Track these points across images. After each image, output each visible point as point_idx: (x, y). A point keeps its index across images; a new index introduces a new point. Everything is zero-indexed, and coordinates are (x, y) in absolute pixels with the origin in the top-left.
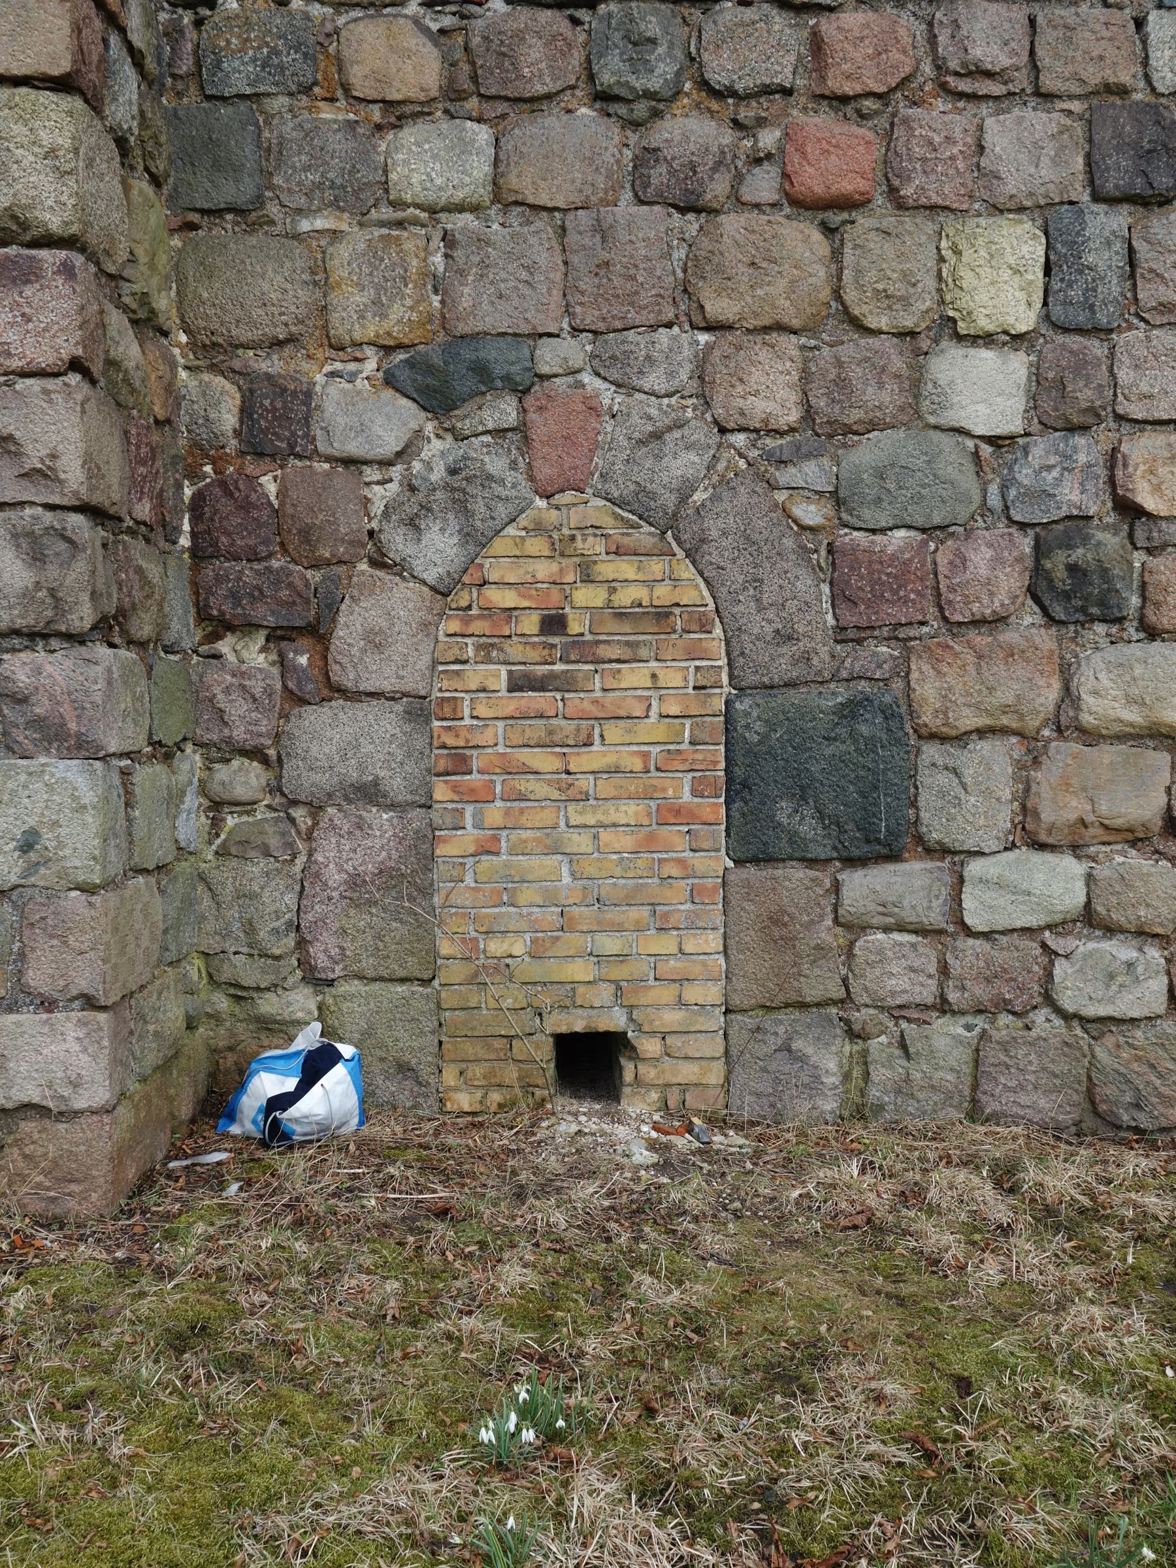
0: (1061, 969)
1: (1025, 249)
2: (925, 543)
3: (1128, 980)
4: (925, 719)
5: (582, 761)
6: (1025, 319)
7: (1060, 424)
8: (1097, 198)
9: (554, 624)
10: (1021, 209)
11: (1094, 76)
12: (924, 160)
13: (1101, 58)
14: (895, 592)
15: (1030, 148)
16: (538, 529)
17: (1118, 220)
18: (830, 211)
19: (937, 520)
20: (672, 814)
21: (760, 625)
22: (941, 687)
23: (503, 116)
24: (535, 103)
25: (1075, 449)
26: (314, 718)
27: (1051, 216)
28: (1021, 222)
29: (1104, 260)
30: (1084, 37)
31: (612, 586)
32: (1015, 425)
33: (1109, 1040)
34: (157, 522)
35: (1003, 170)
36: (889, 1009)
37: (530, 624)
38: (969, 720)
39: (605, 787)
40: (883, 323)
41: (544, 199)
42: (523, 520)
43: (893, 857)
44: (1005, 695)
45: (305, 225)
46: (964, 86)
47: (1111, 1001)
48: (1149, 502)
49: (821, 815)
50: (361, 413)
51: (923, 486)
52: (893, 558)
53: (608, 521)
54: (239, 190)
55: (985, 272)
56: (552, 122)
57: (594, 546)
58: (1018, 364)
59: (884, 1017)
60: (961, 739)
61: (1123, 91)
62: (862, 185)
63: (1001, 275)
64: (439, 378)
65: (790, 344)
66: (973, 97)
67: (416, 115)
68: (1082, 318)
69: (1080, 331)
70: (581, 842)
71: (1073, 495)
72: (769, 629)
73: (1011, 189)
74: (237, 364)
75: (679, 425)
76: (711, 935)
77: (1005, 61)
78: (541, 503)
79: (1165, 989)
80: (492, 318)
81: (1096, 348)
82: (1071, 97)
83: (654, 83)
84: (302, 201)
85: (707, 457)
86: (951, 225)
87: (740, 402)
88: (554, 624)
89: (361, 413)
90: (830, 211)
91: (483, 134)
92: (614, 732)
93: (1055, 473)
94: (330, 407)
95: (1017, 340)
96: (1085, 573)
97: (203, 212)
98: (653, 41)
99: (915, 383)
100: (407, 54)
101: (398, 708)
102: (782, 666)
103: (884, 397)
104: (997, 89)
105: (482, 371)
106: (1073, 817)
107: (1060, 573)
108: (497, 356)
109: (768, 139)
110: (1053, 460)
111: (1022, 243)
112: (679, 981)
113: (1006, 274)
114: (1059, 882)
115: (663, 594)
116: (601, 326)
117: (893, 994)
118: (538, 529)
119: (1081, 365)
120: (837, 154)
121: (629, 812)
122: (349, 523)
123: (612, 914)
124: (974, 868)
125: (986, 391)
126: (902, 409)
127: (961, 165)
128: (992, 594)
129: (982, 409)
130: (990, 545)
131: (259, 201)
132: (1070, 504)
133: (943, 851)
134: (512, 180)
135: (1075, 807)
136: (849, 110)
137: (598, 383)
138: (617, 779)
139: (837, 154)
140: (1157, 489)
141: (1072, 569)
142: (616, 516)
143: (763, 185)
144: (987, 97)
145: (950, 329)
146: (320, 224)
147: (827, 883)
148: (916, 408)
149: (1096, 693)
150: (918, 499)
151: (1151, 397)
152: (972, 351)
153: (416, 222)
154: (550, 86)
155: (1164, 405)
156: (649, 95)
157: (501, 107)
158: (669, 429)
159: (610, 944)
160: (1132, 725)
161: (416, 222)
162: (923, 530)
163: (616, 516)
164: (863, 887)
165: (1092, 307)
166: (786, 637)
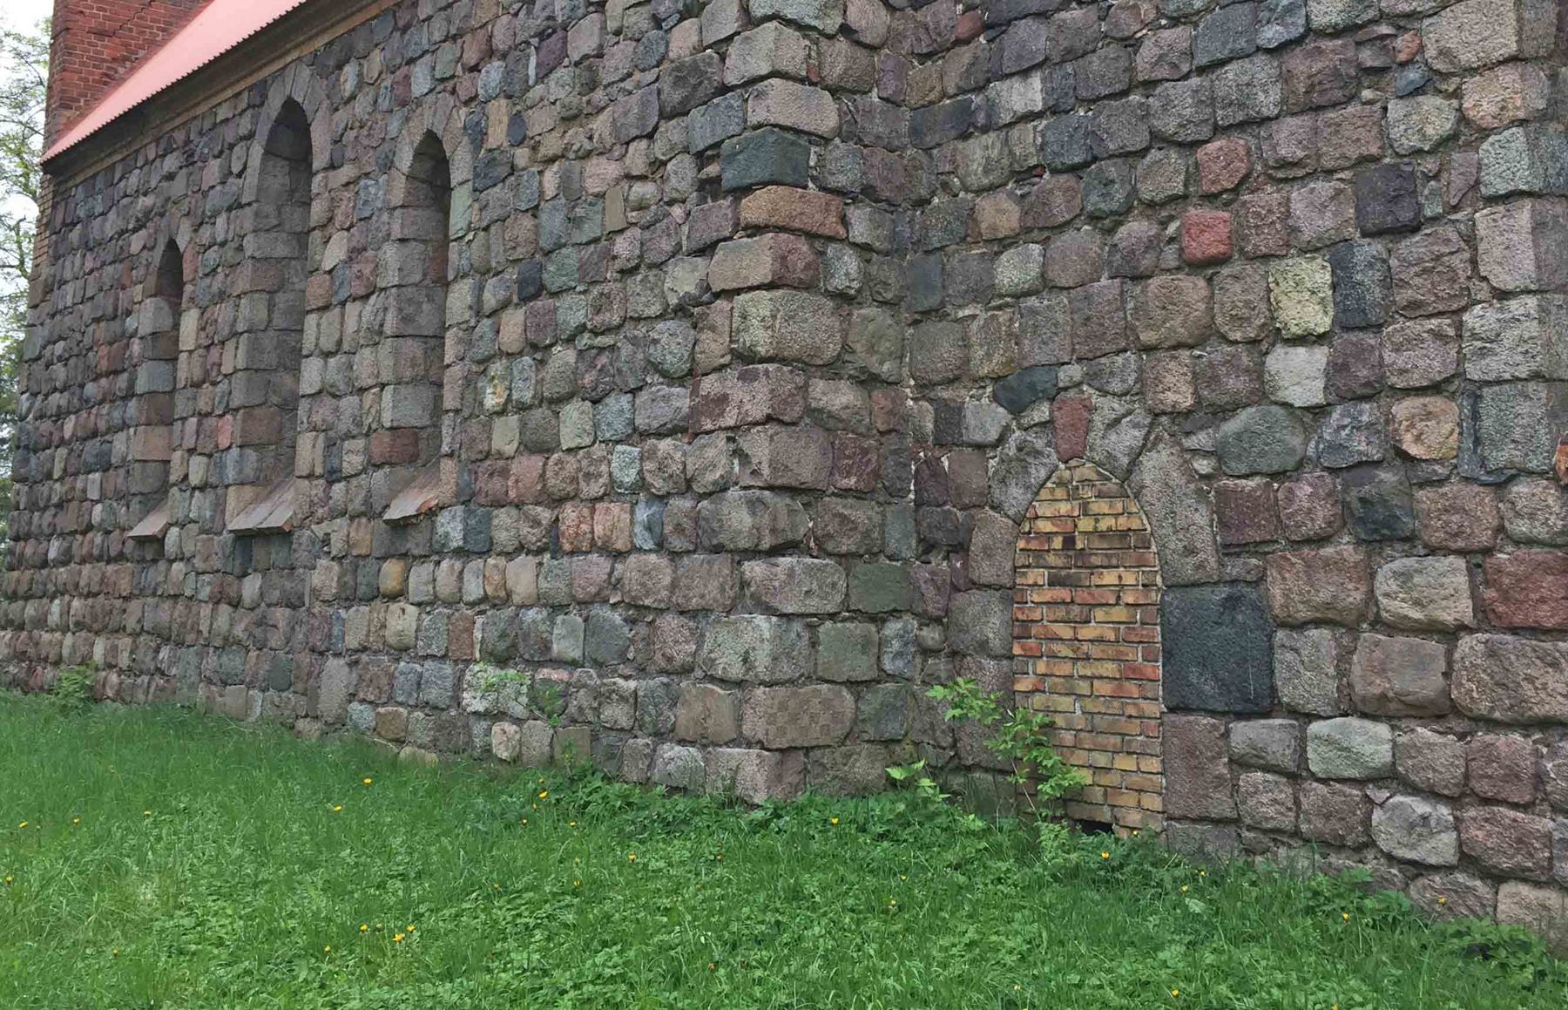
0: (1377, 815)
1: (1318, 276)
2: (1268, 485)
3: (1425, 831)
4: (1277, 612)
5: (1086, 632)
6: (1321, 321)
7: (1349, 395)
8: (1364, 235)
9: (1069, 541)
10: (1317, 250)
11: (1353, 152)
12: (1257, 227)
13: (1358, 140)
14: (1252, 520)
15: (1314, 208)
16: (1061, 483)
17: (1375, 248)
18: (1207, 266)
19: (1275, 468)
20: (1131, 673)
21: (1175, 544)
22: (1285, 588)
23: (1048, 238)
24: (1062, 227)
25: (1361, 413)
26: (960, 599)
27: (1335, 251)
28: (1314, 258)
29: (1368, 278)
30: (1347, 130)
31: (1097, 517)
32: (1319, 398)
33: (1422, 881)
34: (1552, 877)
35: (1300, 223)
36: (1265, 831)
37: (1057, 543)
38: (1304, 614)
39: (1095, 651)
40: (1238, 336)
41: (1064, 283)
42: (1054, 479)
43: (1267, 715)
44: (1324, 595)
45: (961, 314)
46: (1280, 175)
47: (1413, 847)
48: (1414, 450)
49: (1215, 676)
50: (985, 416)
51: (1267, 444)
52: (1249, 495)
53: (1095, 477)
54: (932, 301)
55: (1294, 295)
56: (1068, 237)
57: (1087, 493)
58: (1320, 356)
59: (1266, 840)
60: (1301, 626)
61: (1375, 159)
62: (1222, 248)
63: (1305, 294)
64: (1015, 393)
65: (1184, 354)
66: (1286, 180)
67: (1010, 245)
68: (1358, 321)
69: (1361, 329)
70: (1084, 688)
71: (1362, 446)
72: (1180, 545)
73: (1306, 237)
74: (932, 395)
75: (1129, 413)
76: (1154, 760)
77: (1300, 154)
78: (1062, 466)
79: (1455, 844)
80: (1040, 357)
81: (1370, 339)
82: (1343, 169)
83: (1115, 206)
84: (961, 301)
85: (1144, 431)
86: (1274, 265)
87: (1161, 396)
88: (1069, 541)
89: (985, 416)
90: (1207, 266)
91: (1036, 249)
92: (1099, 614)
93: (1347, 431)
94: (969, 414)
95: (1321, 339)
96: (1372, 503)
97: (922, 313)
98: (1112, 182)
99: (1258, 372)
100: (1004, 212)
101: (998, 594)
102: (1188, 569)
103: (1236, 384)
104: (1300, 173)
105: (1032, 387)
106: (1377, 691)
107: (1356, 505)
108: (1040, 377)
109: (1172, 229)
110: (1347, 421)
111: (1318, 274)
112: (1140, 791)
113: (1307, 295)
114: (1373, 741)
115: (1123, 523)
116: (1090, 355)
117: (1267, 819)
118: (1061, 483)
119: (1361, 352)
120: (1207, 228)
121: (1109, 669)
122: (977, 482)
123: (1101, 739)
124: (1316, 727)
125: (1300, 375)
126: (1252, 392)
127: (1278, 226)
128: (1312, 520)
129: (1298, 389)
130: (1310, 485)
131: (943, 304)
132: (1360, 453)
133: (1293, 712)
134: (1050, 275)
135: (1379, 686)
136: (1218, 203)
137: (1091, 391)
138: (1102, 647)
139: (1207, 228)
140: (1418, 439)
141: (1361, 500)
142: (1099, 473)
143: (1170, 256)
144: (1295, 179)
145: (1276, 336)
146: (967, 312)
147: (1222, 729)
148: (1262, 393)
149: (1387, 595)
150: (1262, 454)
151: (1407, 371)
152: (1291, 350)
153: (1007, 305)
154: (1068, 217)
155: (1416, 376)
156: (1112, 213)
157: (1046, 234)
158: (1124, 416)
159: (1101, 760)
160: (1416, 621)
161: (1007, 305)
162: (1268, 475)
163: (1099, 473)
164: (1245, 733)
165: (1363, 311)
166: (1190, 551)
